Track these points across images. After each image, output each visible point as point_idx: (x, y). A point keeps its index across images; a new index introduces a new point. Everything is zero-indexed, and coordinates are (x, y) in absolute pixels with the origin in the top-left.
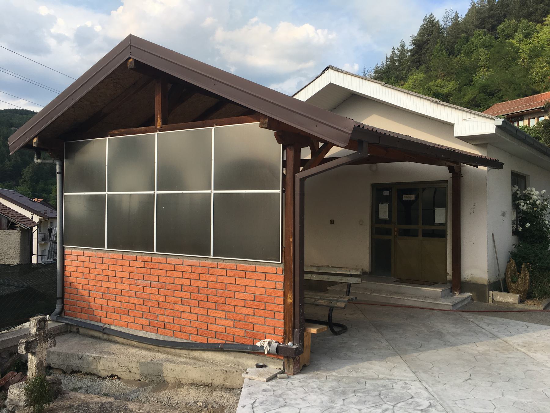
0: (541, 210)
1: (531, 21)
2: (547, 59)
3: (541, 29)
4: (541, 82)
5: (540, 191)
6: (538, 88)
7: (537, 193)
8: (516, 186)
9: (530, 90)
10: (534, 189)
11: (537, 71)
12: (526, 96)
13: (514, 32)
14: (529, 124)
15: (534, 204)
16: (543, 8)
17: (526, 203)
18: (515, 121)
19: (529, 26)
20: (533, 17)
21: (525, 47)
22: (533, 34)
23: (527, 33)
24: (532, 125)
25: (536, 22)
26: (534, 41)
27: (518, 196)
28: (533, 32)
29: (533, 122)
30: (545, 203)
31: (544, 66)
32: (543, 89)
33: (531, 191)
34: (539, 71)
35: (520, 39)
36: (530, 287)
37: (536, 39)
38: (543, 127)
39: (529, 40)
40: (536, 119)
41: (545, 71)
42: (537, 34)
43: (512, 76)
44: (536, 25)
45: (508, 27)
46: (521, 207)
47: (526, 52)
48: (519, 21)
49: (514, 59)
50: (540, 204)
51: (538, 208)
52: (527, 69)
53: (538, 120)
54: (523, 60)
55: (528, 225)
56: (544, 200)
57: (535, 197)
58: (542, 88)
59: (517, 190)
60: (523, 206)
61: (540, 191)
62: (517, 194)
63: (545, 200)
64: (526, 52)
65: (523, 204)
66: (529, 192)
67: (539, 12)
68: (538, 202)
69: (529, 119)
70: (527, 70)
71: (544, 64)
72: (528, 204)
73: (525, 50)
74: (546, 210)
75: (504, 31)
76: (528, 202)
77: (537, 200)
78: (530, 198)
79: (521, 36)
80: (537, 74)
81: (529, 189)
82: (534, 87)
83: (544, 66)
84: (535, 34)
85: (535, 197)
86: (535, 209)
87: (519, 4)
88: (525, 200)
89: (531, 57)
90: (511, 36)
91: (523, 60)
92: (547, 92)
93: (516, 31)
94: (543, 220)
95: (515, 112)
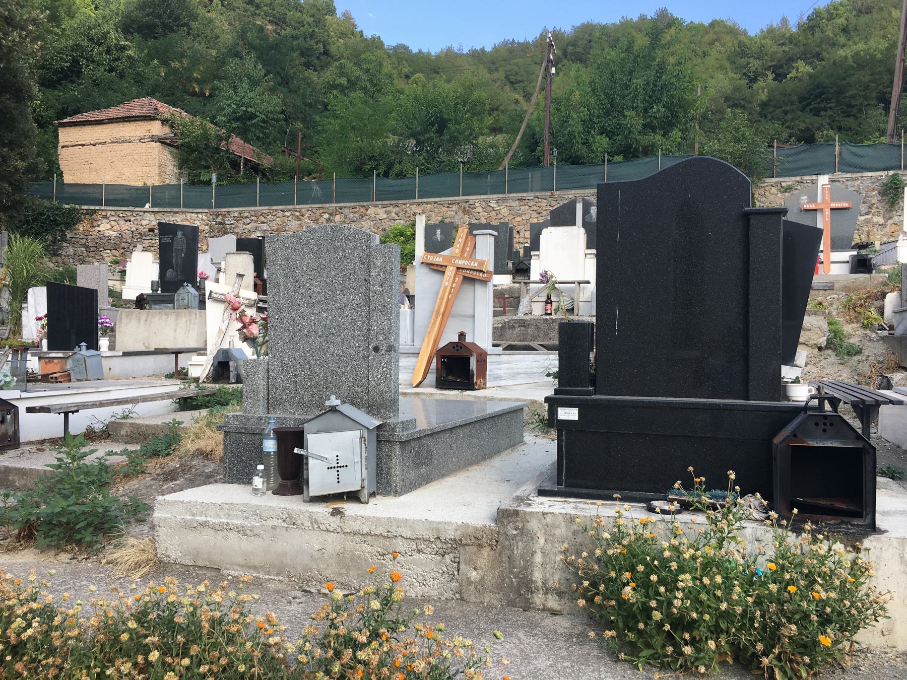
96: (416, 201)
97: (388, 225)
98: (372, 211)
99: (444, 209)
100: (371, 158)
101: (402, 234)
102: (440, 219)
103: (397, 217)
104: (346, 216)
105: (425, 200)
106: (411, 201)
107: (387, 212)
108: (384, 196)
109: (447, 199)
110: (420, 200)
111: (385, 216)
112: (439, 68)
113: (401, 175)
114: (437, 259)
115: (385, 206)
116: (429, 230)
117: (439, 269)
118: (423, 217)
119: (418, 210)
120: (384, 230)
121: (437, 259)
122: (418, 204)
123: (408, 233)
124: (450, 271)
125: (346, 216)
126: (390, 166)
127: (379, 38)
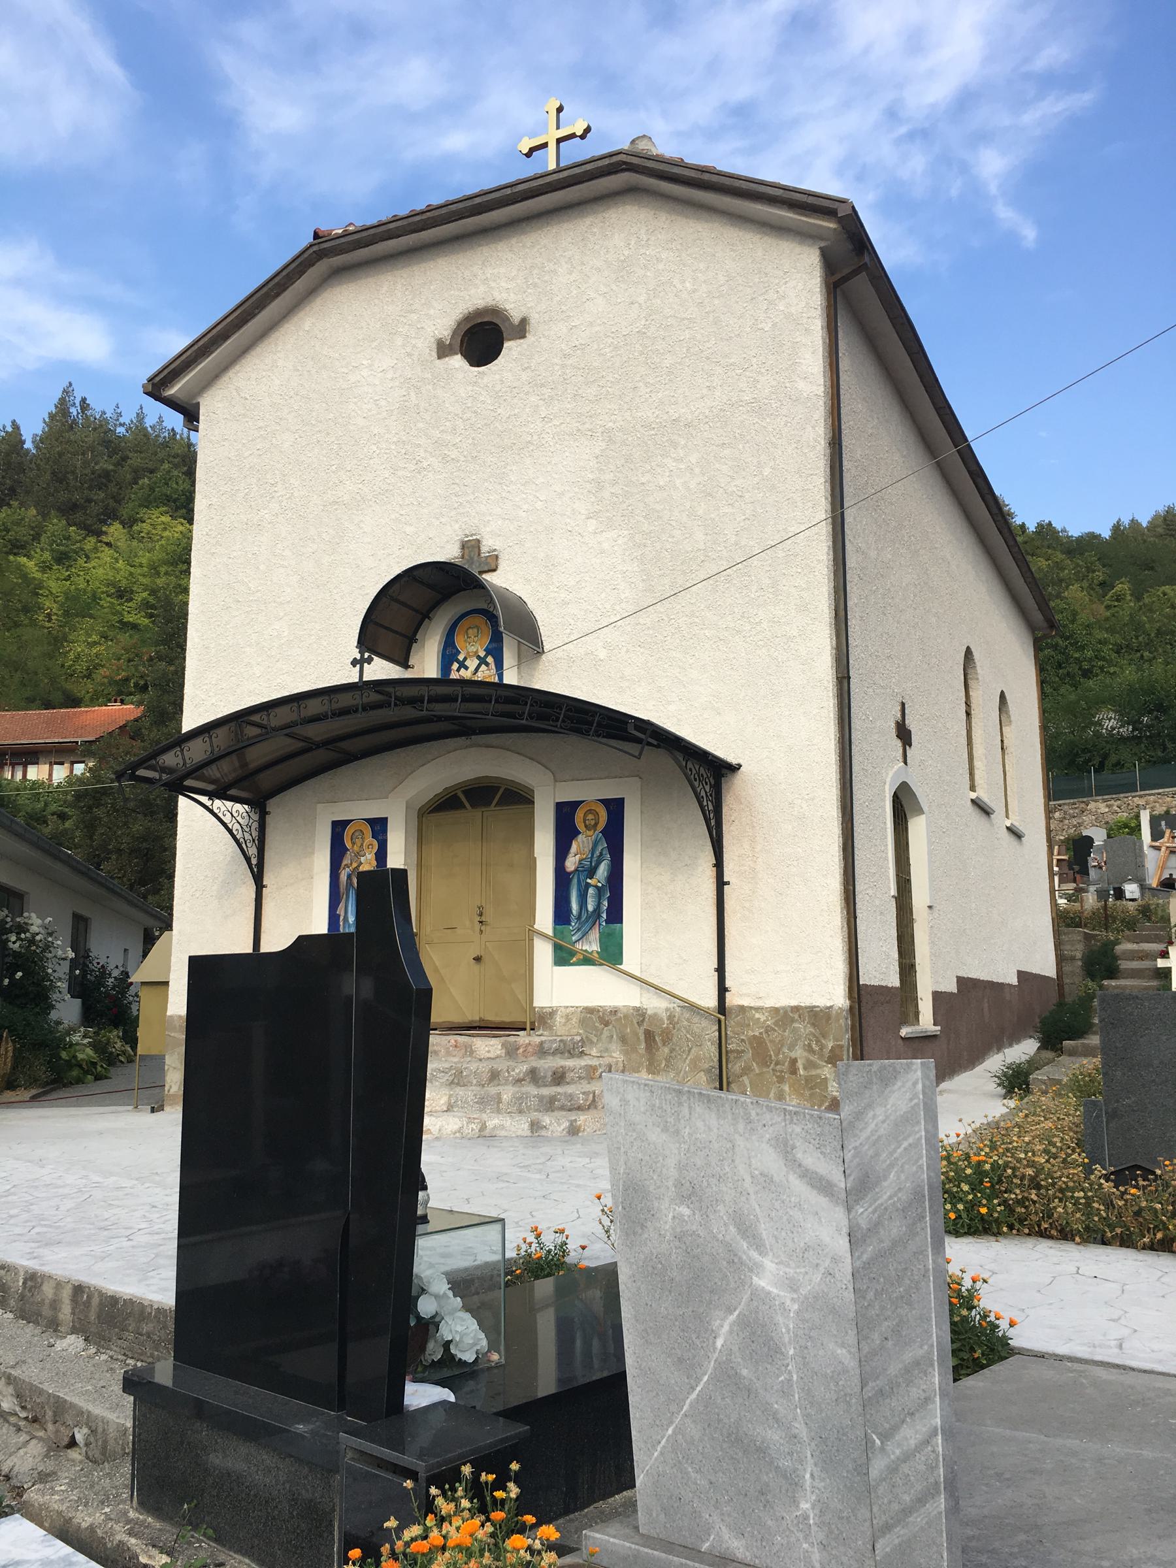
0: (44, 951)
1: (75, 524)
2: (103, 627)
3: (96, 549)
4: (85, 676)
5: (43, 921)
6: (84, 688)
7: (39, 922)
8: (5, 909)
9: (60, 693)
10: (33, 915)
11: (79, 650)
12: (48, 705)
13: (33, 540)
14: (50, 775)
15: (32, 941)
16: (103, 501)
17: (19, 939)
18: (19, 764)
19: (68, 538)
20: (79, 516)
21: (54, 583)
22: (75, 560)
23: (62, 553)
24: (55, 781)
25: (85, 529)
26: (79, 576)
27: (8, 926)
28: (77, 553)
29: (60, 774)
30: (50, 939)
31: (95, 643)
32: (90, 695)
33: (29, 918)
34: (83, 651)
35: (44, 562)
36: (14, 1068)
37: (82, 573)
38: (73, 796)
39: (67, 571)
40: (67, 765)
41: (97, 655)
42: (86, 562)
43: (19, 649)
44: (84, 538)
45: (18, 523)
46: (11, 945)
47: (57, 597)
48: (45, 516)
49: (26, 609)
50: (41, 941)
51: (38, 946)
52: (56, 639)
53: (72, 771)
54: (49, 615)
55: (20, 974)
56: (48, 933)
57: (34, 929)
58: (88, 692)
59: (7, 916)
60: (14, 943)
61: (43, 921)
62: (7, 923)
63: (50, 934)
64: (57, 597)
65: (13, 938)
66: (26, 921)
67: (94, 509)
68: (38, 938)
69: (51, 764)
70: (57, 641)
71: (95, 638)
72: (22, 940)
73: (54, 592)
74: (50, 952)
75: (8, 531)
76: (23, 936)
77: (37, 934)
78: (26, 931)
79: (47, 555)
80: (78, 657)
81: (26, 914)
82: (68, 686)
83: (95, 643)
84: (81, 561)
85: (34, 929)
86: (34, 948)
87: (48, 476)
88: (18, 934)
89: (67, 614)
90: (23, 547)
91: (49, 615)
92: (96, 708)
93: (36, 537)
94: (44, 968)
95: (18, 742)
96: (1138, 793)
97: (1110, 818)
98: (1092, 806)
99: (1169, 799)
100: (1084, 751)
101: (1126, 826)
102: (1165, 809)
103: (1119, 810)
104: (1065, 813)
105: (1148, 792)
106: (1133, 794)
107: (1108, 806)
108: (1104, 790)
109: (1171, 789)
110: (1142, 793)
111: (1107, 810)
112: (1153, 561)
113: (1118, 765)
114: (1157, 844)
115: (1105, 801)
116: (1154, 821)
117: (1158, 848)
118: (1148, 811)
119: (1141, 802)
120: (1107, 823)
121: (1157, 844)
122: (1140, 796)
123: (1133, 825)
124: (1163, 849)
125: (1065, 813)
126: (1105, 756)
127: (1050, 524)
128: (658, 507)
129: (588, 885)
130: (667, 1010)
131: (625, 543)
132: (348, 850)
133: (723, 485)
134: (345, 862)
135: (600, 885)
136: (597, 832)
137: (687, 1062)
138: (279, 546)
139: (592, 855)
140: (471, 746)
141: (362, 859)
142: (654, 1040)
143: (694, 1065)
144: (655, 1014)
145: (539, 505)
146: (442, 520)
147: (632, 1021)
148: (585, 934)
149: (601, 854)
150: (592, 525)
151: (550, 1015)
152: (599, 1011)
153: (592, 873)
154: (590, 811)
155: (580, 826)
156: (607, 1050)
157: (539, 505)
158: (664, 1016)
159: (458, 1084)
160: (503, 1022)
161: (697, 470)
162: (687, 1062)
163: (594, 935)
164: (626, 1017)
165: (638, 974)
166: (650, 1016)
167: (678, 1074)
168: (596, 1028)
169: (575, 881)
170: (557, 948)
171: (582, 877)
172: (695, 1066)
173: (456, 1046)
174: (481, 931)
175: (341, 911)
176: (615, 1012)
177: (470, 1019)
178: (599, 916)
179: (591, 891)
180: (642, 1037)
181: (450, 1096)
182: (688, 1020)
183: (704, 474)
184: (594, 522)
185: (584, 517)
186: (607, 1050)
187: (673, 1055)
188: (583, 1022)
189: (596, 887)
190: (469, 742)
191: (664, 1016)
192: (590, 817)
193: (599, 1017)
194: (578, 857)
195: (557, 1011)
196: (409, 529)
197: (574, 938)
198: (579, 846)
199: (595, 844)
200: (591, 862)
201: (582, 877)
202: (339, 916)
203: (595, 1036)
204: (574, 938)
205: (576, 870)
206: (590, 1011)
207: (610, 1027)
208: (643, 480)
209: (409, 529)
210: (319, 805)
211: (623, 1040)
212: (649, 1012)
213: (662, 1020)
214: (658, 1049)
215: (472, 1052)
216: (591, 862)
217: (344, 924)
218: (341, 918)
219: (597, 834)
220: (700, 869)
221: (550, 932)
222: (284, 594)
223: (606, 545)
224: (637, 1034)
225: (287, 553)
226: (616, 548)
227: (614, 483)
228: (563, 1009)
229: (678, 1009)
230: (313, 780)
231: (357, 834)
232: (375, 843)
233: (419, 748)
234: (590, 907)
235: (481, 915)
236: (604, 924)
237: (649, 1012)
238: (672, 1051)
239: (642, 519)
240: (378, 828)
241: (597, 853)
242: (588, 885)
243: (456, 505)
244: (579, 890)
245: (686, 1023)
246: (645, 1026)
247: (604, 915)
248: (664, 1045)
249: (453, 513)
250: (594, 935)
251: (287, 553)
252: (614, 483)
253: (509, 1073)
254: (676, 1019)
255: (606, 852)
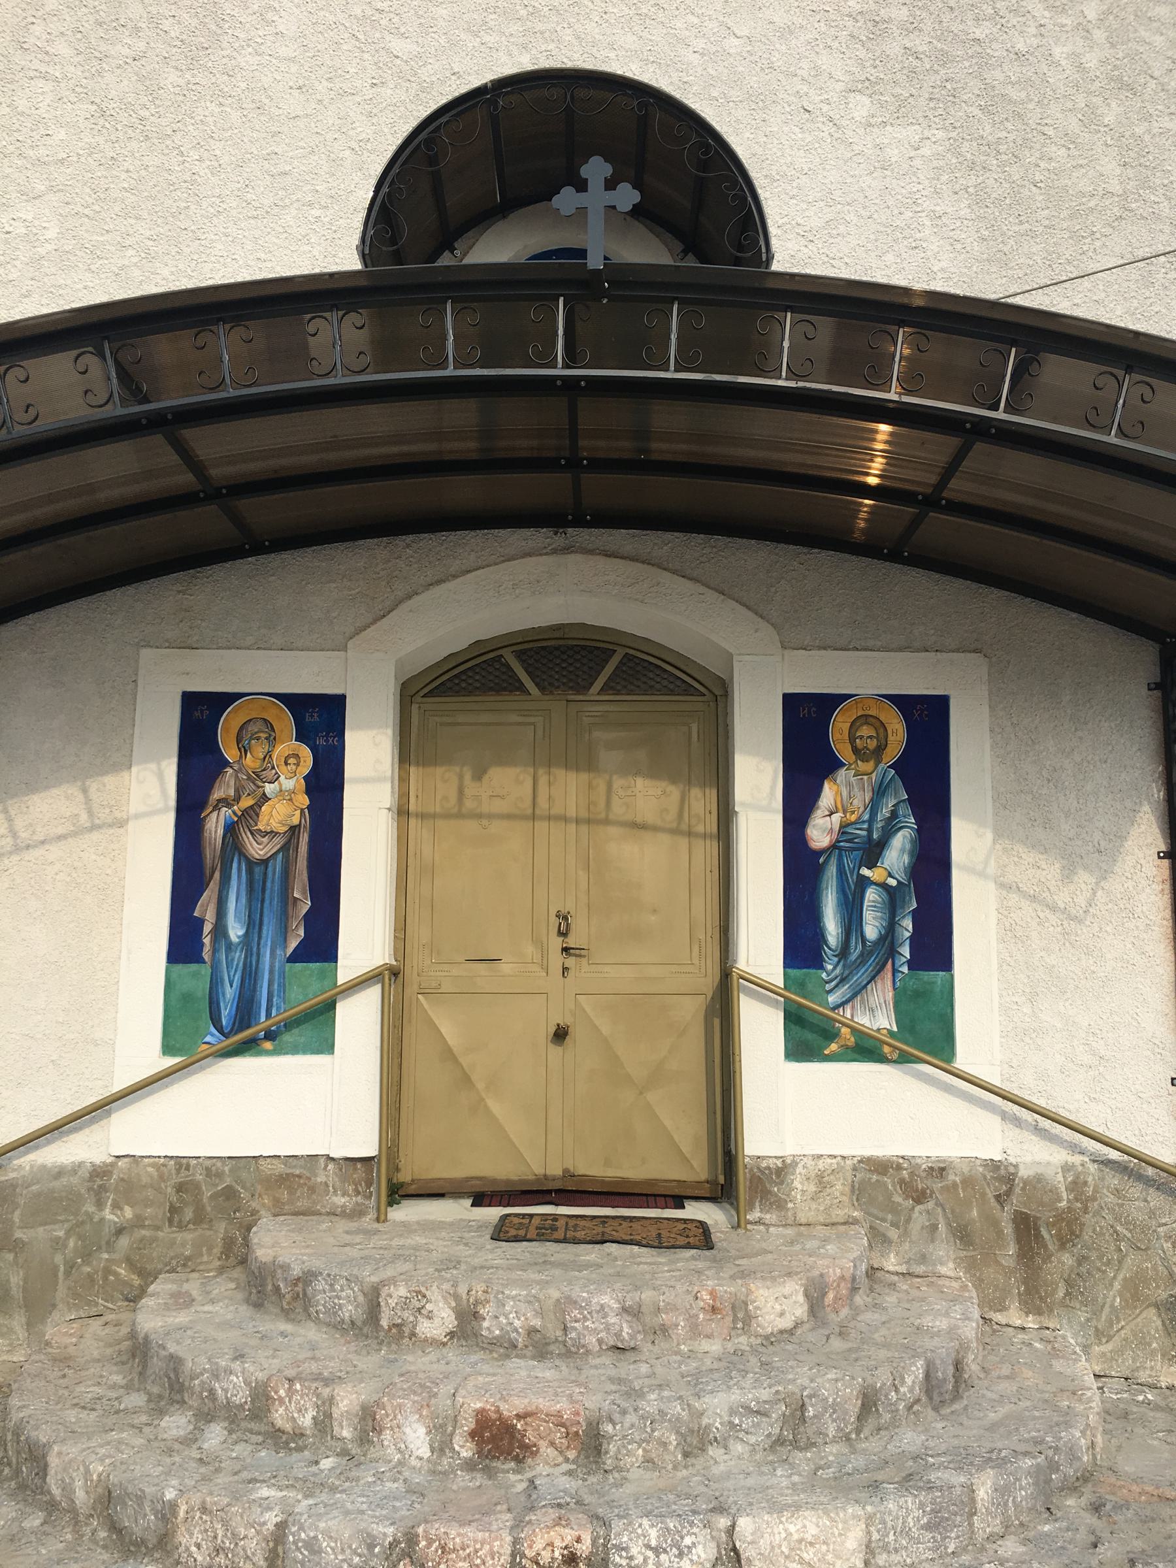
128: (1014, 93)
129: (864, 882)
130: (1066, 1168)
131: (938, 156)
132: (226, 764)
133: (1156, 74)
134: (217, 794)
135: (893, 882)
136: (881, 766)
137: (1117, 1285)
138: (37, 29)
139: (871, 821)
140: (567, 550)
141: (269, 788)
142: (1038, 1235)
143: (1134, 1293)
144: (1039, 1178)
145: (732, 45)
146: (487, 38)
147: (983, 1195)
148: (859, 991)
149: (894, 814)
150: (861, 106)
151: (778, 1175)
152: (899, 1167)
153: (873, 852)
154: (865, 719)
155: (842, 749)
156: (923, 1259)
157: (732, 45)
158: (1060, 1182)
159: (795, 1444)
160: (625, 1181)
161: (1099, 35)
162: (1117, 1285)
163: (882, 993)
164: (968, 1182)
165: (996, 1081)
166: (1026, 1182)
167: (1097, 1313)
168: (894, 1209)
169: (832, 871)
170: (795, 1018)
171: (848, 863)
172: (1136, 1296)
173: (714, 1310)
174: (565, 969)
175: (206, 909)
176: (939, 1170)
177: (539, 1171)
178: (893, 952)
179: (871, 895)
180: (1008, 1229)
181: (870, 1519)
182: (1117, 1192)
183: (1113, 45)
184: (866, 100)
185: (840, 86)
186: (923, 1259)
187: (1083, 1270)
188: (860, 1192)
189: (884, 886)
190: (559, 541)
191: (1060, 1182)
192: (865, 731)
193: (902, 1181)
194: (836, 818)
195: (795, 1164)
196: (398, 45)
197: (832, 999)
198: (839, 793)
199: (880, 792)
200: (870, 830)
201: (848, 863)
202: (201, 922)
203: (895, 1225)
204: (832, 999)
205: (833, 847)
206: (880, 1166)
207: (930, 1205)
208: (978, 33)
209: (398, 45)
210: (146, 653)
211: (963, 1235)
212: (1023, 1173)
213: (1054, 1191)
214: (1048, 1258)
215: (748, 1319)
216: (870, 830)
217: (215, 941)
218: (207, 928)
219: (883, 769)
220: (1130, 861)
221: (780, 983)
222: (49, 141)
223: (893, 154)
224: (995, 1223)
225: (62, 49)
226: (917, 163)
227: (912, 27)
228: (810, 1163)
229: (1093, 1168)
230: (130, 590)
231: (253, 728)
232: (306, 753)
233: (428, 541)
234: (871, 931)
235: (564, 934)
236: (905, 969)
237: (1023, 1173)
238: (1082, 1260)
239: (977, 112)
240: (312, 717)
241: (885, 812)
242: (864, 882)
243: (523, 12)
244: (842, 890)
245: (1111, 1199)
246: (1016, 1202)
247: (906, 951)
248: (1062, 1246)
249: (515, 28)
250: (882, 993)
251: (62, 49)
252: (912, 27)
253: (897, 1390)
254: (1090, 1191)
255: (905, 811)
